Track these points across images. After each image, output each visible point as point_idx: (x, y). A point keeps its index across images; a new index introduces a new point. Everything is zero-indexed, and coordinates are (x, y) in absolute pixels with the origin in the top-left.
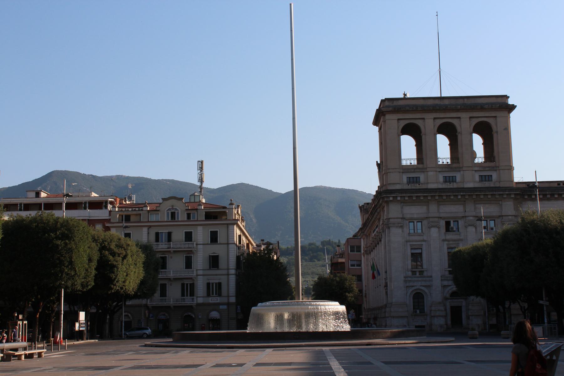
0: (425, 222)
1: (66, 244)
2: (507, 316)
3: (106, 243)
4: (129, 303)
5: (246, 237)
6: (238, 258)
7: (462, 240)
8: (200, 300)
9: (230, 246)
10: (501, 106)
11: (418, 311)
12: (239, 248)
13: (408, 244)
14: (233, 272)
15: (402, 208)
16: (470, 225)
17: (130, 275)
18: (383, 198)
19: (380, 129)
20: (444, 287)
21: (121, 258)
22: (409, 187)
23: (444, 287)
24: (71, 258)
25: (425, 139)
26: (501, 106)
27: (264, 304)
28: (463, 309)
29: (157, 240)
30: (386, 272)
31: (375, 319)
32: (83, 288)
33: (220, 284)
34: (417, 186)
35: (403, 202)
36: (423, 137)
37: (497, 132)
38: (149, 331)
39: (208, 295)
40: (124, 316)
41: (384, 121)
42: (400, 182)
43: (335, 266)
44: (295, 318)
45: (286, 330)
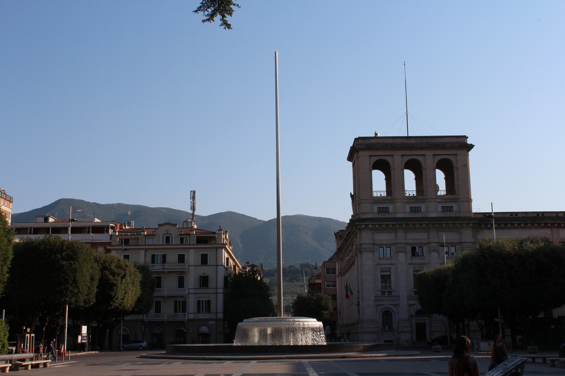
0: (393, 248)
1: (71, 264)
3: (107, 264)
4: (127, 318)
5: (233, 260)
6: (226, 278)
7: (426, 264)
8: (191, 316)
9: (219, 267)
10: (461, 145)
11: (387, 328)
12: (227, 269)
13: (412, 266)
14: (221, 291)
16: (400, 251)
17: (128, 293)
18: (356, 226)
19: (354, 164)
21: (120, 278)
22: (380, 216)
23: (410, 305)
24: (75, 277)
26: (461, 145)
27: (248, 320)
29: (153, 261)
30: (358, 292)
31: (348, 334)
33: (209, 302)
34: (387, 216)
36: (392, 172)
37: (457, 168)
38: (144, 344)
39: (199, 312)
42: (372, 211)
43: (313, 286)
44: (277, 333)
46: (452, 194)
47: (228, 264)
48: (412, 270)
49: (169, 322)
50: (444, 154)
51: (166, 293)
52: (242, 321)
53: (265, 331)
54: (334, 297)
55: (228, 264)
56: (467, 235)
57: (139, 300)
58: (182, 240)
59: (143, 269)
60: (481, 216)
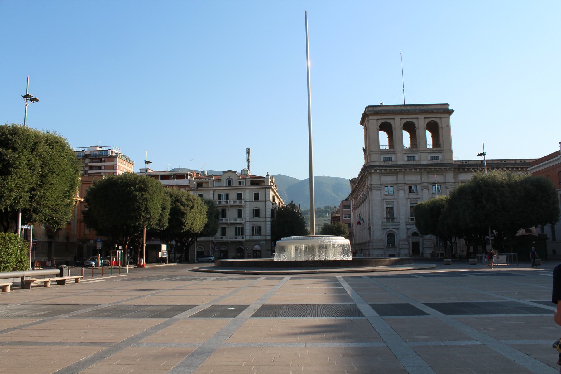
0: (395, 187)
1: (142, 195)
2: (454, 247)
3: (179, 198)
4: (199, 239)
5: (278, 198)
6: (272, 211)
7: (419, 198)
8: (248, 238)
9: (267, 202)
10: (444, 111)
11: (391, 245)
12: (273, 204)
14: (269, 219)
15: (380, 177)
16: (400, 189)
17: (196, 220)
18: (368, 171)
19: (365, 127)
20: (408, 229)
21: (189, 208)
22: (385, 163)
23: (408, 229)
24: (146, 205)
25: (395, 132)
26: (444, 111)
27: (285, 238)
28: (420, 244)
29: (219, 199)
30: (369, 220)
31: (361, 250)
32: (160, 228)
33: (260, 228)
34: (390, 163)
35: (381, 174)
36: (394, 131)
37: (442, 128)
38: (213, 258)
39: (253, 235)
40: (195, 248)
41: (368, 121)
42: (379, 160)
43: (334, 219)
44: (311, 250)
45: (304, 259)
46: (437, 147)
47: (274, 201)
48: (409, 203)
49: (232, 243)
50: (432, 117)
51: (229, 221)
52: (280, 239)
53: (300, 248)
54: (349, 225)
55: (274, 201)
56: (450, 177)
57: (207, 226)
58: (240, 183)
59: (209, 203)
60: (460, 163)
